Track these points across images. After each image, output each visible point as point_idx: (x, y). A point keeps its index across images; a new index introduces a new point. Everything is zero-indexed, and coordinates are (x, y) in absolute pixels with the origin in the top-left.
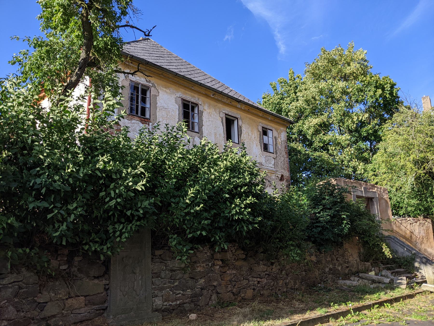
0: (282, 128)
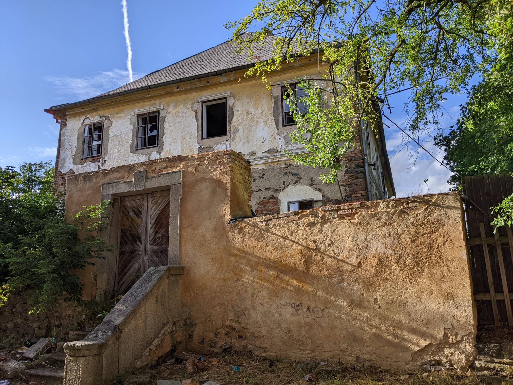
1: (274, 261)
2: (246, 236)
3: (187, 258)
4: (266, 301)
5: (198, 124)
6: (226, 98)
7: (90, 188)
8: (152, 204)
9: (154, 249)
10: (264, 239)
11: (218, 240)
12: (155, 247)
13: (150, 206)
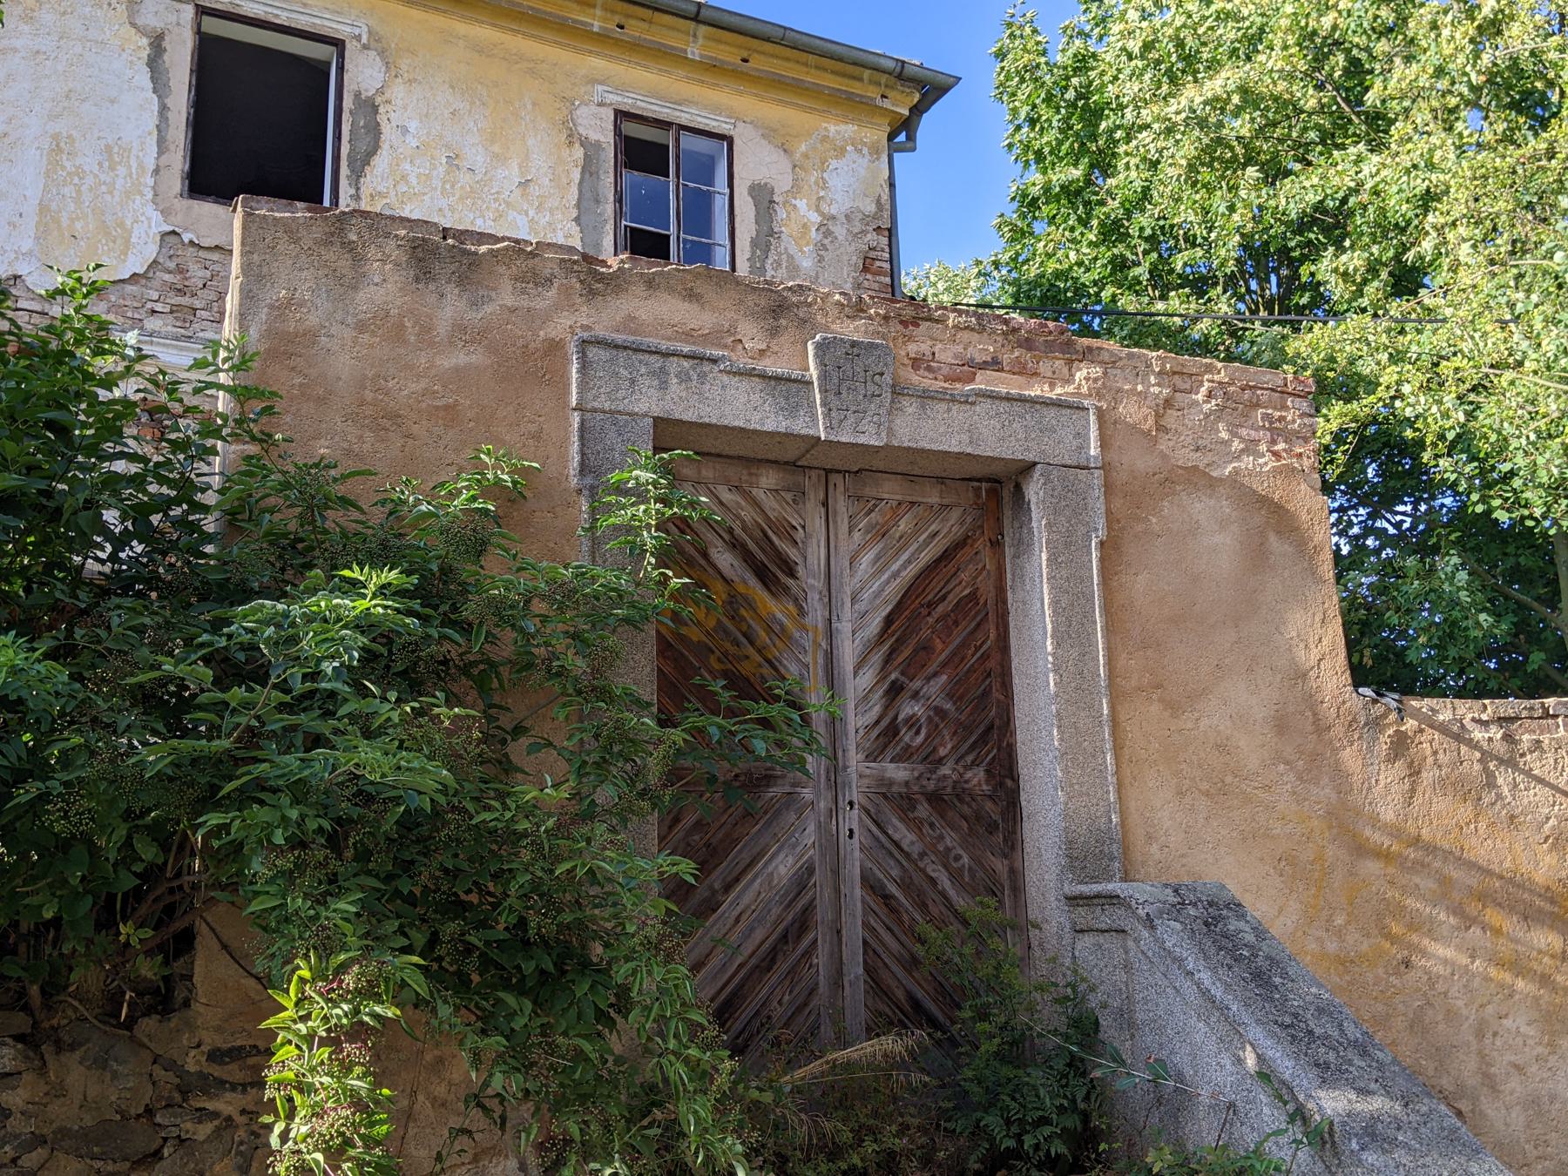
0: (840, 129)
1: (1548, 888)
2: (1424, 774)
3: (1154, 848)
4: (1535, 1053)
5: (163, 109)
6: (339, 44)
7: (462, 334)
8: (857, 535)
9: (891, 783)
10: (1499, 797)
11: (1300, 778)
12: (899, 773)
13: (846, 543)
